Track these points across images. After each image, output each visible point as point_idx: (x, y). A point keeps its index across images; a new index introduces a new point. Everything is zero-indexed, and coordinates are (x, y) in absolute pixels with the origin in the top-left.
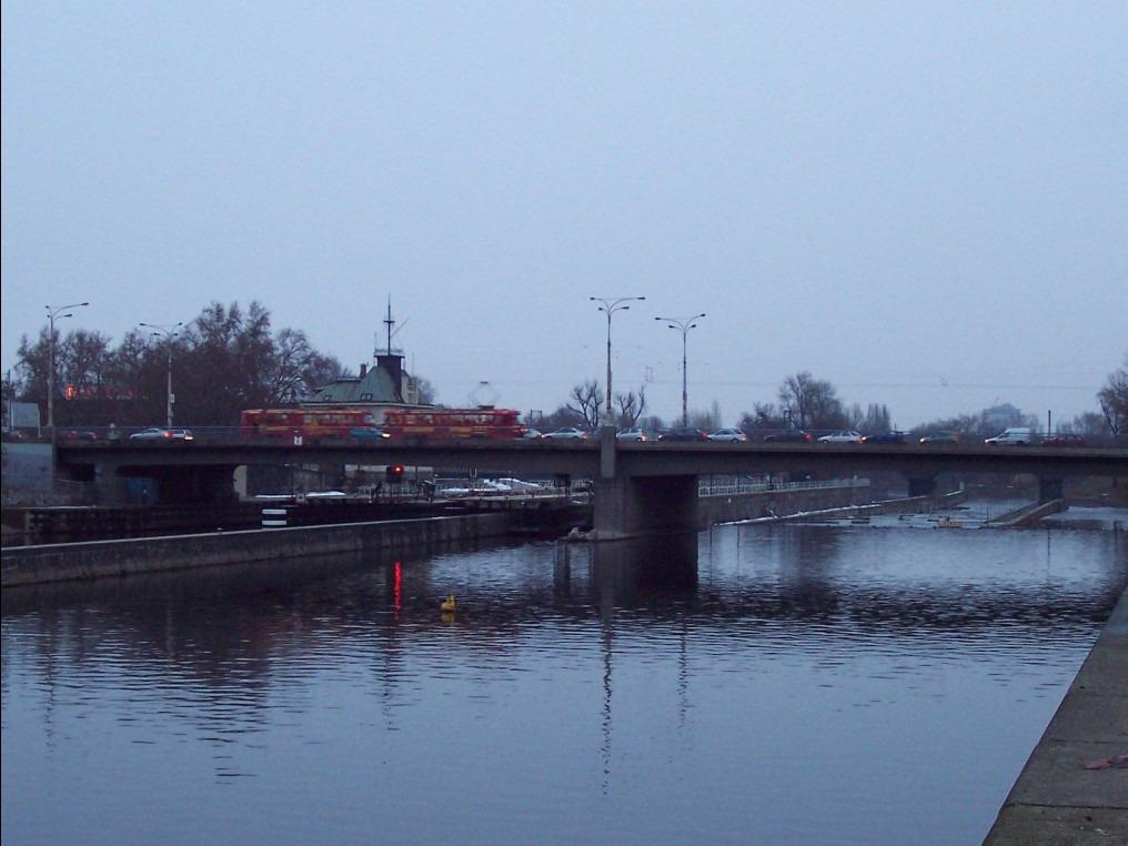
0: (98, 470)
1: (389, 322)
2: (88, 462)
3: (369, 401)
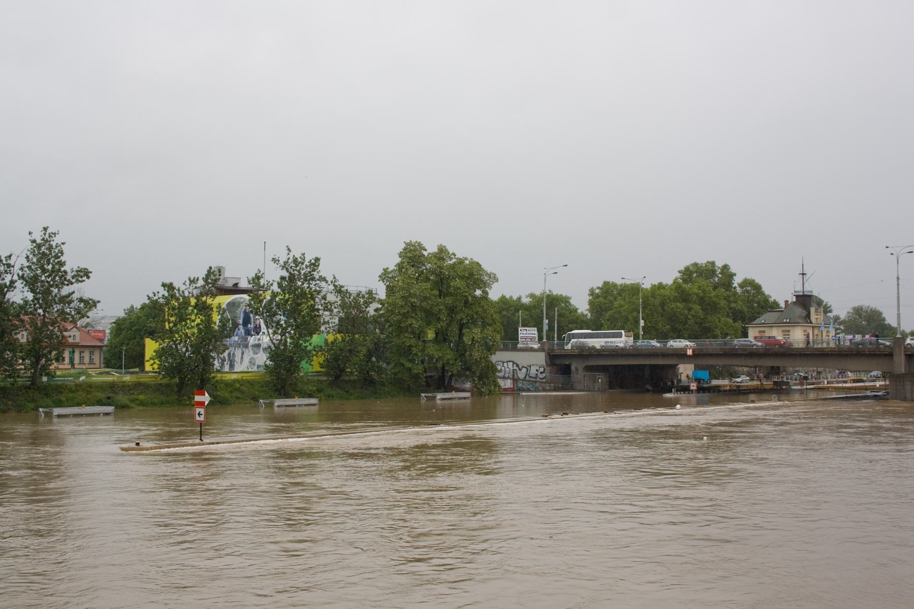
0: (573, 368)
1: (803, 274)
2: (567, 363)
3: (789, 323)
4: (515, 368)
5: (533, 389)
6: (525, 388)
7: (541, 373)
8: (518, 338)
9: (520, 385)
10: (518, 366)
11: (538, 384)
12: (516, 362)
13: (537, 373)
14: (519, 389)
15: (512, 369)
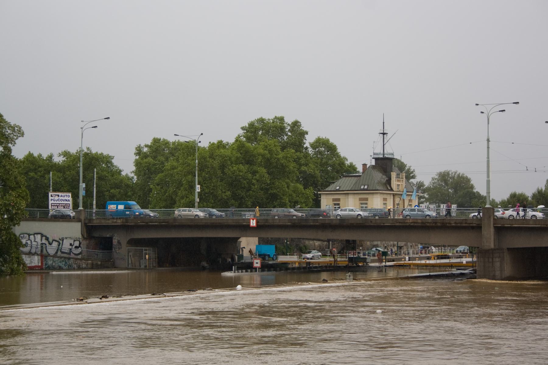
4: (44, 241)
7: (76, 247)
9: (50, 263)
10: (47, 239)
11: (71, 261)
12: (44, 234)
13: (71, 247)
15: (40, 242)
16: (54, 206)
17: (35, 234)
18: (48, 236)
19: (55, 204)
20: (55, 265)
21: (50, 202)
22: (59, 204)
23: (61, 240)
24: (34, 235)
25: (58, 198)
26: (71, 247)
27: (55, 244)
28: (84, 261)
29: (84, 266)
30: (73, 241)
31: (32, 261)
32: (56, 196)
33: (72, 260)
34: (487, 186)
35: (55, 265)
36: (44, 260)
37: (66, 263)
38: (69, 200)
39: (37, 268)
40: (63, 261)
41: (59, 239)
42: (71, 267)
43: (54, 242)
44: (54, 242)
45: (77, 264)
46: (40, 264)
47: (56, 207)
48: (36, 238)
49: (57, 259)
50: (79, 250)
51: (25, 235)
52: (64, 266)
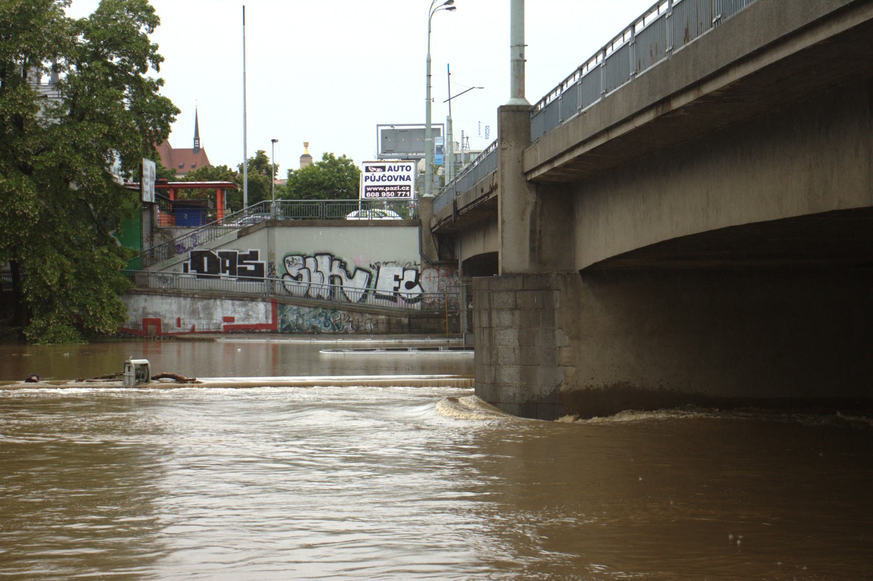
4: (336, 270)
5: (326, 330)
6: (306, 325)
7: (409, 285)
8: (357, 188)
9: (292, 318)
10: (343, 265)
11: (340, 315)
12: (337, 255)
13: (396, 284)
14: (289, 326)
15: (327, 274)
16: (371, 192)
17: (317, 255)
18: (344, 259)
19: (374, 187)
20: (303, 324)
21: (363, 184)
22: (385, 187)
23: (373, 268)
24: (314, 257)
25: (381, 174)
26: (398, 282)
27: (360, 280)
28: (370, 316)
29: (369, 326)
30: (401, 269)
31: (250, 313)
32: (379, 169)
33: (341, 312)
34: (513, 13)
35: (303, 324)
36: (279, 312)
37: (327, 319)
38: (408, 176)
39: (264, 330)
40: (320, 315)
41: (371, 266)
42: (339, 328)
43: (358, 272)
44: (358, 272)
45: (352, 321)
46: (270, 322)
47: (378, 194)
48: (319, 263)
49: (307, 310)
50: (417, 290)
51: (297, 257)
52: (323, 327)
